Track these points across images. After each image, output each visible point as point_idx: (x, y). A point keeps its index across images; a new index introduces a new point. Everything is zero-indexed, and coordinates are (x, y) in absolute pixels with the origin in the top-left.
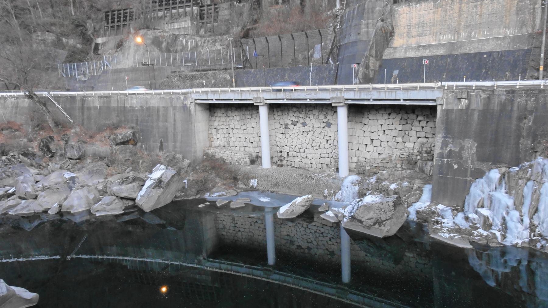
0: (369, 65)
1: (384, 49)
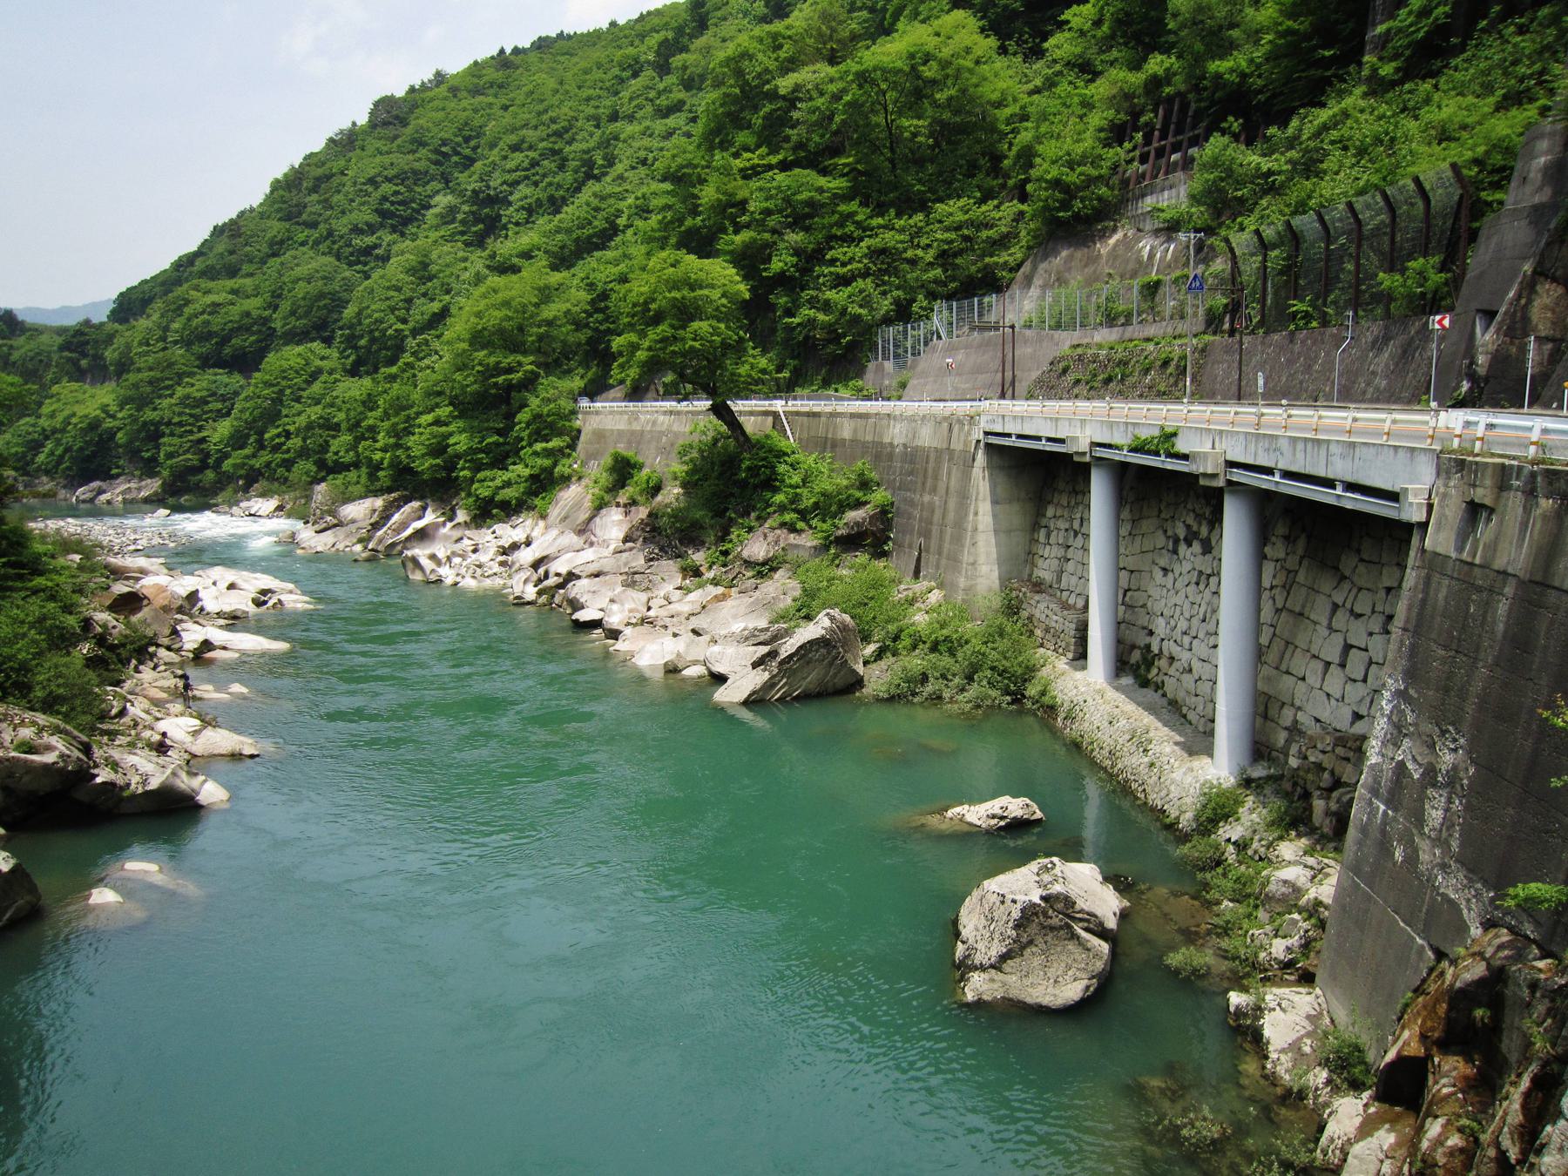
0: (1526, 319)
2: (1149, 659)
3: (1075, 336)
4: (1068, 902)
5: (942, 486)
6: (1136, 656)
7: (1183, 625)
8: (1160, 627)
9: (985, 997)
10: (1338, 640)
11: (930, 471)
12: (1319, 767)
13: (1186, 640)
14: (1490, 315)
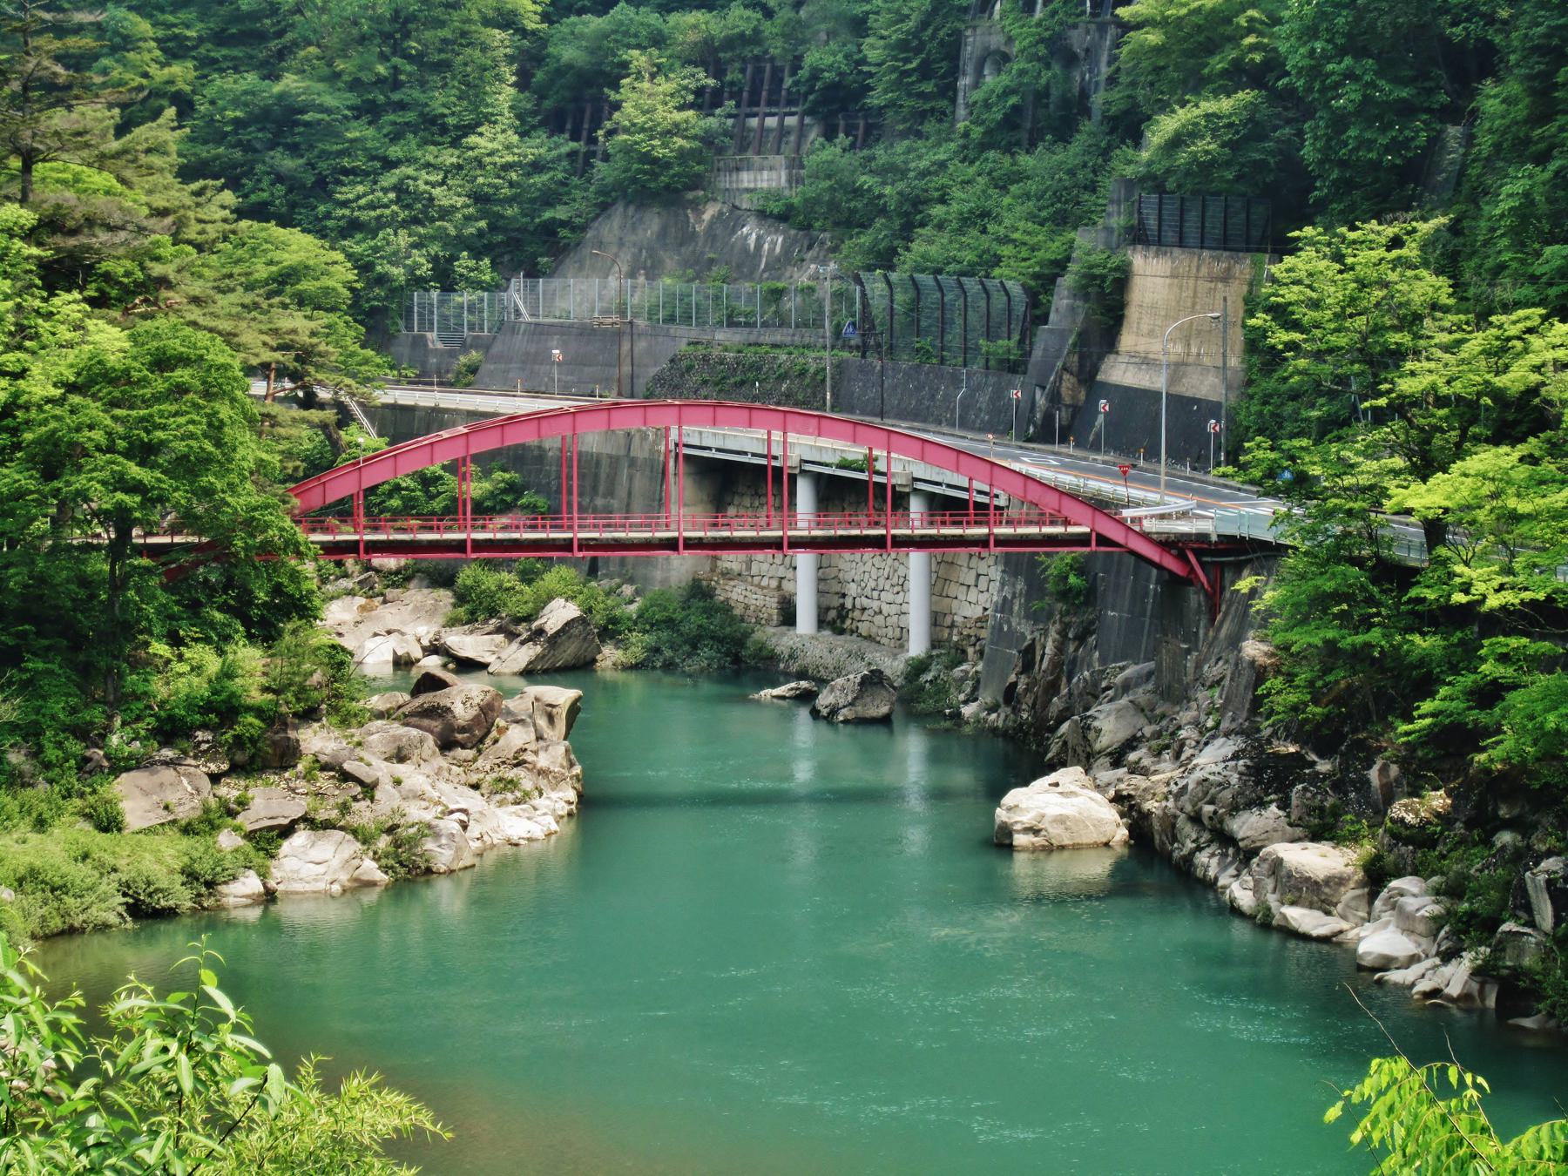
0: (1059, 393)
1: (1101, 358)
2: (843, 613)
3: (693, 332)
4: (881, 672)
5: (622, 492)
6: (832, 614)
7: (872, 584)
8: (852, 589)
9: (1112, 357)
10: (974, 574)
11: (603, 476)
12: (969, 636)
13: (875, 594)
14: (1043, 388)
